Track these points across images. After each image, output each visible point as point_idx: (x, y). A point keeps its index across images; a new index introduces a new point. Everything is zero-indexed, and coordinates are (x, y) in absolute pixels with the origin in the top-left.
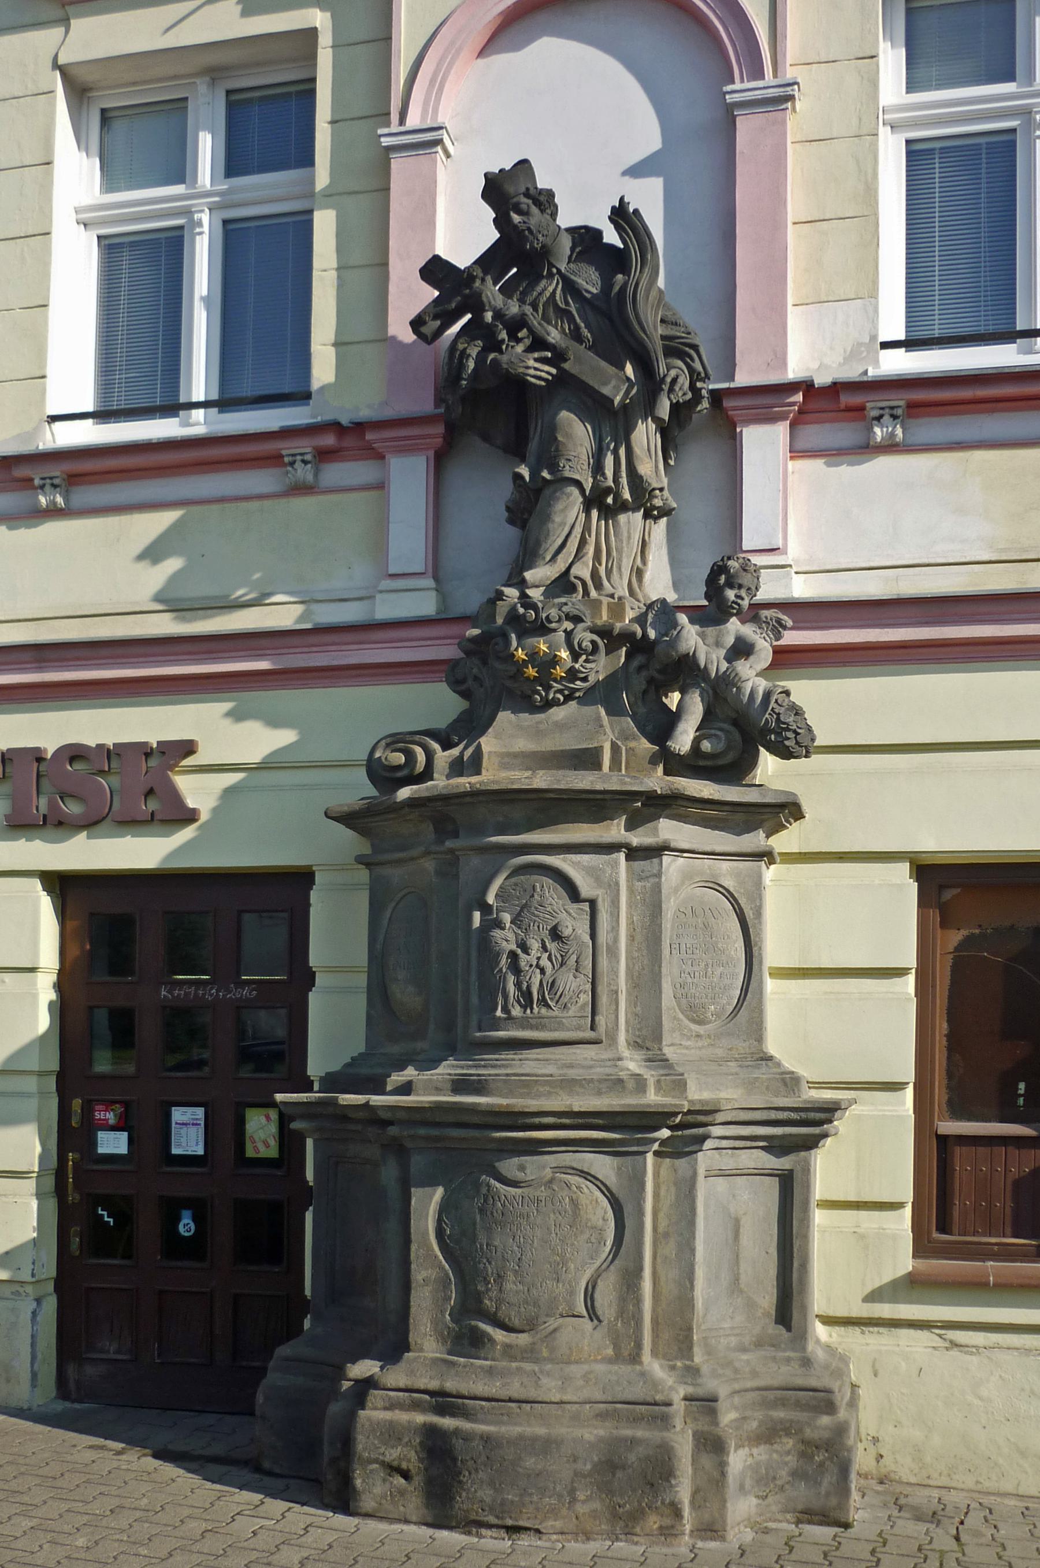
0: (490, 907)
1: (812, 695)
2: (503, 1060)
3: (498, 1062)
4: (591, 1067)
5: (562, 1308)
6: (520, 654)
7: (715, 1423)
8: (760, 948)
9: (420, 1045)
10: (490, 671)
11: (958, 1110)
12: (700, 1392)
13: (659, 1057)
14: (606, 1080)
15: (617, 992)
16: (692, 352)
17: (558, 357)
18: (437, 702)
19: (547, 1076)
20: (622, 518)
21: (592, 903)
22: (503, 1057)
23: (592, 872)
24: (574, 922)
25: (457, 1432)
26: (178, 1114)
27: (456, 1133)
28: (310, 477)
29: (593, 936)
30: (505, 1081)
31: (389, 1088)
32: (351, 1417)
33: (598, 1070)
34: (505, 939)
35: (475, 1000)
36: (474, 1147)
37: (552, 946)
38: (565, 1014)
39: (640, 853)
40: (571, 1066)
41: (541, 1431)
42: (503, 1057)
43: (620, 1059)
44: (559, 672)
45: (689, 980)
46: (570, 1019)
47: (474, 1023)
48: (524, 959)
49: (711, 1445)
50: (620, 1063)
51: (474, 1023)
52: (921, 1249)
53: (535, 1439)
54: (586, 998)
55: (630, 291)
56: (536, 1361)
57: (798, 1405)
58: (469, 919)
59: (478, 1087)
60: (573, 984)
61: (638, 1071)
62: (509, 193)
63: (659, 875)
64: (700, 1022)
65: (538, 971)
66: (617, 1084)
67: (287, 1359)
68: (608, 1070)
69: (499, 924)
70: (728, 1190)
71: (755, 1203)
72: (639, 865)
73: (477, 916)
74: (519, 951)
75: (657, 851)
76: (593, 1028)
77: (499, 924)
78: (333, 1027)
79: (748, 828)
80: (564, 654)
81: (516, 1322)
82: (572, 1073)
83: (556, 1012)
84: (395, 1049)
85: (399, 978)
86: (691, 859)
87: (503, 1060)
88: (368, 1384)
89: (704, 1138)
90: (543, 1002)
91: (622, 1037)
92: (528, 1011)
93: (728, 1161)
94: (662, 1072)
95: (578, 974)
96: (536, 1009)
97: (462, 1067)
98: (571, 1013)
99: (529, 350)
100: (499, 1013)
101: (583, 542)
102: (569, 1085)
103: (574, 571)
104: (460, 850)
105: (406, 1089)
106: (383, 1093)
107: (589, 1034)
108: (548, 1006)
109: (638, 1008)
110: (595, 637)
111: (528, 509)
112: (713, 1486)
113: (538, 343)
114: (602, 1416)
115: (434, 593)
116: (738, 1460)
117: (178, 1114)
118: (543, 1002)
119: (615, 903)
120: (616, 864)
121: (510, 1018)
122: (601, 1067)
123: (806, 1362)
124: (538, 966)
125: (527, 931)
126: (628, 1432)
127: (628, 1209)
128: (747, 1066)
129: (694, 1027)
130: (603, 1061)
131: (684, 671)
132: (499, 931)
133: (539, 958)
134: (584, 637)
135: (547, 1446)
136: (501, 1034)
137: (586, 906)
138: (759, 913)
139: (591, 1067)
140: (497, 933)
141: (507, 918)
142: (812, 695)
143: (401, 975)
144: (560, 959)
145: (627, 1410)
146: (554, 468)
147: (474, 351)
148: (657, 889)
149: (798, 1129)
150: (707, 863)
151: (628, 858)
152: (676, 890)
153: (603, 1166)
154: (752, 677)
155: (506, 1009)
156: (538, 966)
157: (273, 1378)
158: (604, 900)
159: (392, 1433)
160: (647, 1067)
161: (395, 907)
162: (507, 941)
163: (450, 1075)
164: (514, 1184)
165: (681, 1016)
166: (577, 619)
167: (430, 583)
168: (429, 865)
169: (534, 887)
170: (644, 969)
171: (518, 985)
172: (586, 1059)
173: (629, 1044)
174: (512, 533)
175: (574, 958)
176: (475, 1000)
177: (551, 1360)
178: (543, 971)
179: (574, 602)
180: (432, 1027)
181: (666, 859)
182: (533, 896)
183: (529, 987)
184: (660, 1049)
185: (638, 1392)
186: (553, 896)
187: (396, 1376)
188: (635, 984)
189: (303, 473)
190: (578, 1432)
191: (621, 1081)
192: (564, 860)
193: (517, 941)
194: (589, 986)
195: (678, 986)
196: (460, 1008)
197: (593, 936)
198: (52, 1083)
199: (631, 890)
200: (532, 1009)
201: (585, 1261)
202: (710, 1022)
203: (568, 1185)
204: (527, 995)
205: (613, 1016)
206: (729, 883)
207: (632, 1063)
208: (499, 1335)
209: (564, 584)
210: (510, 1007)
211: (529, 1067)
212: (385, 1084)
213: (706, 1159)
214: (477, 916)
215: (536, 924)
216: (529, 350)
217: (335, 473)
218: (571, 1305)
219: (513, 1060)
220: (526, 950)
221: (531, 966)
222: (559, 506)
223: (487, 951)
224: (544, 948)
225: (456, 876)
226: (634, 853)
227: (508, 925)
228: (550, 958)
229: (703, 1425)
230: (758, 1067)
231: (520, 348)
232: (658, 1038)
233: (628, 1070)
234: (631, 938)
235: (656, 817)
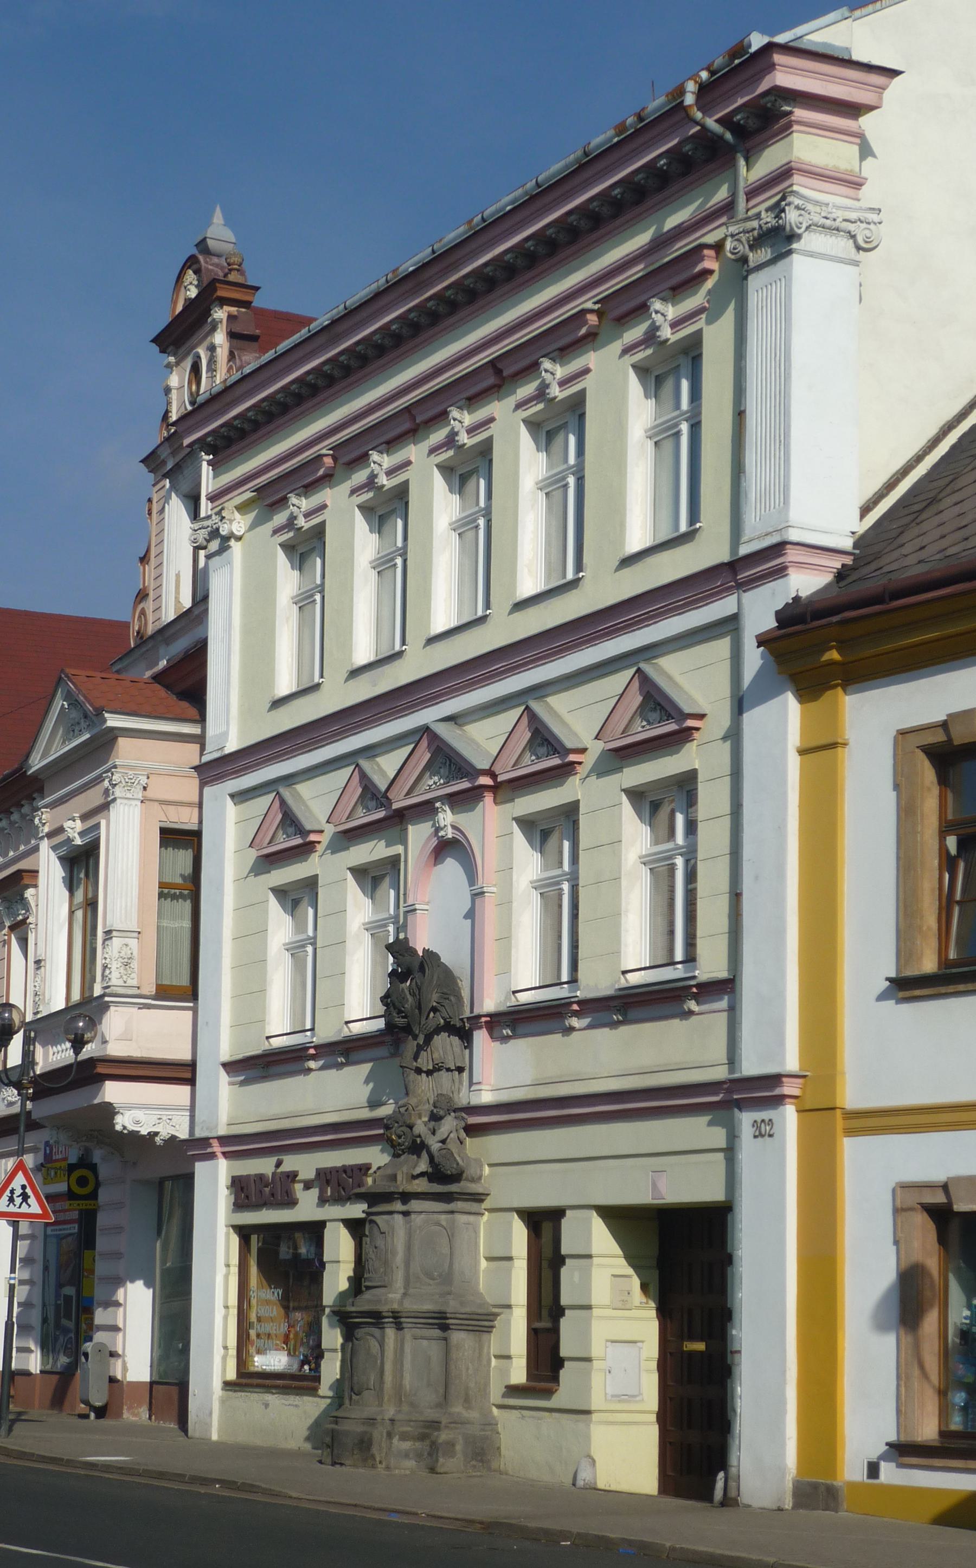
23: (387, 1222)
114: (363, 1424)
153: (376, 1331)
181: (413, 1216)
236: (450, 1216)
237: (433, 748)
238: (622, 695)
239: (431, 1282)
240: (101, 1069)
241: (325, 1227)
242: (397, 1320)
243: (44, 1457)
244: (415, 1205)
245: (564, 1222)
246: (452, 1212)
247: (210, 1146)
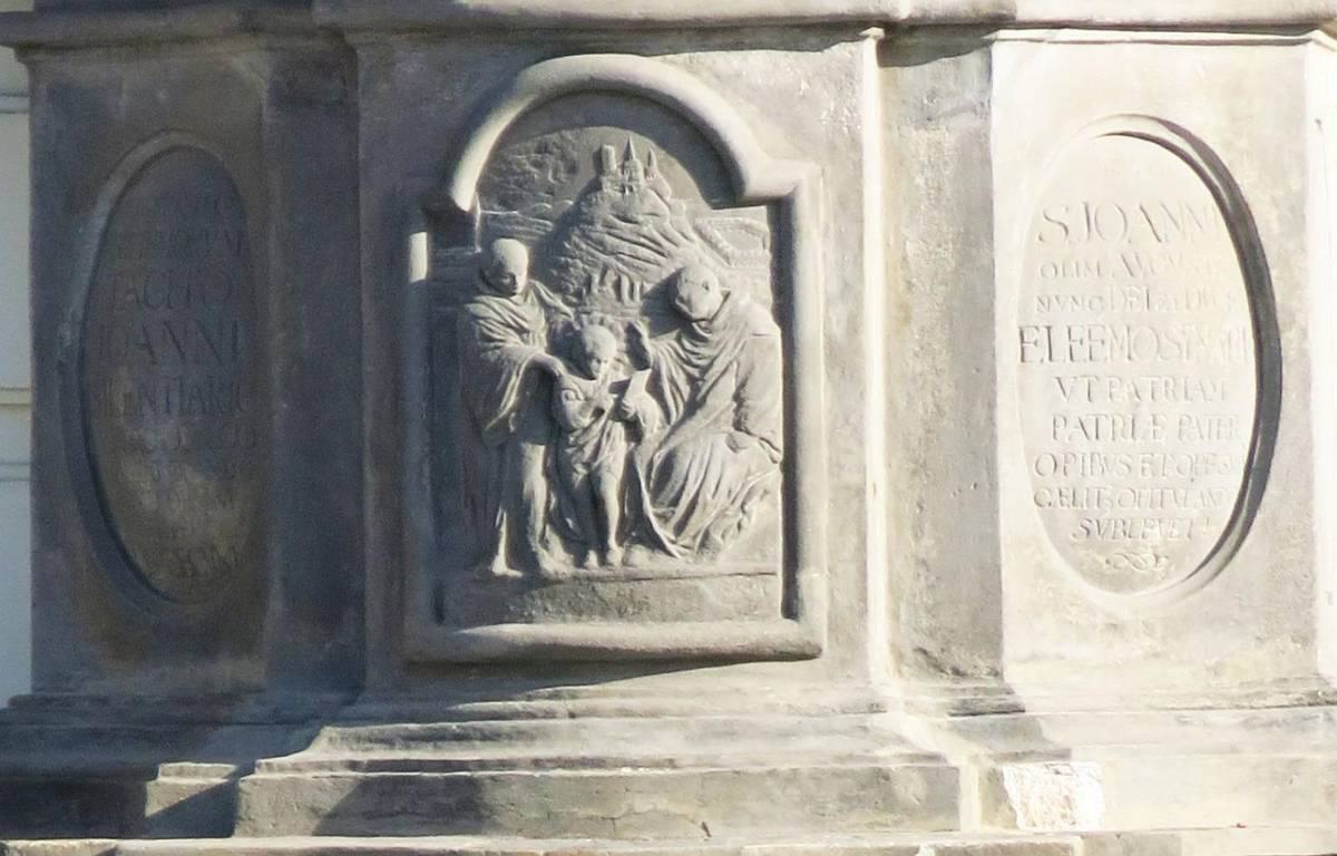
0: (464, 219)
2: (516, 715)
3: (505, 725)
4: (785, 735)
8: (1304, 333)
9: (227, 670)
13: (993, 701)
14: (836, 774)
15: (860, 492)
19: (658, 765)
21: (781, 210)
22: (518, 705)
23: (779, 107)
24: (723, 267)
29: (785, 311)
30: (531, 784)
31: (152, 809)
33: (812, 743)
34: (518, 325)
35: (421, 520)
37: (661, 348)
38: (704, 566)
39: (921, 39)
40: (729, 732)
42: (518, 705)
43: (875, 708)
45: (1083, 446)
46: (712, 582)
47: (420, 598)
48: (576, 393)
50: (876, 718)
51: (420, 598)
54: (767, 512)
60: (729, 469)
61: (930, 747)
63: (982, 109)
64: (1118, 581)
65: (619, 429)
68: (843, 745)
69: (496, 280)
72: (914, 77)
73: (420, 243)
74: (559, 367)
76: (791, 609)
77: (496, 280)
82: (730, 754)
84: (148, 683)
85: (152, 439)
87: (516, 715)
90: (639, 531)
91: (879, 632)
92: (593, 558)
94: (1004, 747)
95: (740, 436)
96: (616, 552)
97: (388, 742)
98: (723, 562)
100: (500, 566)
104: (356, 30)
107: (782, 631)
108: (655, 544)
109: (927, 542)
118: (639, 531)
119: (849, 204)
120: (847, 79)
121: (535, 580)
122: (819, 732)
124: (619, 413)
125: (580, 299)
128: (1270, 724)
130: (823, 712)
132: (494, 301)
133: (621, 388)
136: (514, 631)
137: (758, 218)
138: (1296, 218)
139: (785, 735)
140: (491, 309)
141: (517, 255)
143: (161, 432)
144: (686, 389)
145: (1001, 719)
148: (976, 156)
151: (889, 53)
155: (523, 554)
156: (619, 413)
158: (814, 197)
160: (956, 729)
161: (119, 201)
162: (521, 331)
163: (353, 765)
165: (1057, 562)
167: (25, 103)
168: (250, 64)
169: (599, 160)
170: (940, 411)
171: (557, 473)
172: (771, 708)
173: (899, 657)
175: (729, 385)
176: (421, 520)
178: (634, 430)
180: (276, 605)
181: (1007, 49)
182: (596, 186)
183: (593, 480)
184: (997, 674)
186: (661, 190)
188: (918, 464)
191: (881, 777)
192: (691, 69)
193: (552, 334)
194: (775, 477)
195: (1047, 465)
196: (373, 550)
197: (785, 311)
199: (897, 161)
200: (603, 551)
202: (1148, 581)
205: (852, 568)
207: (915, 719)
210: (536, 546)
211: (601, 737)
212: (141, 798)
214: (420, 243)
215: (611, 277)
219: (550, 715)
220: (582, 362)
221: (599, 412)
224: (638, 357)
225: (346, 111)
227: (522, 281)
228: (655, 388)
230: (1302, 725)
232: (989, 638)
233: (901, 740)
234: (901, 315)
236: (1266, 58)
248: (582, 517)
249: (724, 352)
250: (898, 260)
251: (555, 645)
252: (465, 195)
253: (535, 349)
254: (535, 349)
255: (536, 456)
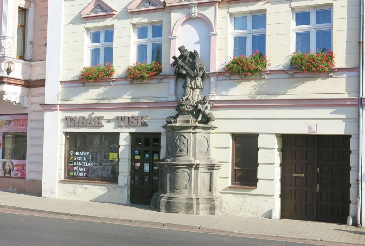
1: (216, 114)
5: (183, 188)
6: (181, 108)
7: (199, 201)
10: (180, 109)
11: (236, 166)
12: (198, 198)
16: (203, 69)
17: (187, 71)
18: (173, 112)
20: (195, 90)
21: (188, 139)
23: (188, 136)
24: (185, 142)
25: (171, 201)
26: (145, 164)
27: (172, 166)
28: (161, 81)
29: (188, 143)
32: (160, 200)
34: (178, 143)
36: (174, 168)
40: (185, 159)
41: (179, 201)
44: (186, 111)
46: (184, 153)
49: (198, 204)
52: (232, 183)
53: (178, 202)
55: (195, 62)
56: (180, 194)
57: (210, 201)
58: (175, 141)
59: (175, 161)
60: (185, 149)
62: (181, 49)
66: (189, 161)
67: (155, 195)
70: (203, 175)
71: (207, 176)
75: (195, 133)
76: (187, 154)
78: (163, 152)
79: (208, 129)
80: (186, 109)
81: (178, 189)
82: (184, 160)
83: (183, 152)
86: (200, 134)
88: (162, 196)
89: (199, 168)
93: (203, 171)
99: (184, 70)
101: (190, 93)
102: (184, 161)
103: (189, 98)
105: (167, 161)
106: (165, 162)
110: (190, 107)
111: (185, 87)
112: (198, 209)
113: (184, 69)
114: (186, 200)
115: (175, 98)
116: (201, 206)
117: (145, 164)
118: (182, 151)
120: (190, 134)
123: (212, 196)
126: (188, 202)
127: (190, 176)
129: (201, 154)
131: (200, 111)
134: (189, 106)
135: (179, 203)
136: (177, 155)
138: (209, 140)
140: (177, 143)
141: (178, 141)
142: (216, 114)
146: (186, 85)
147: (177, 70)
149: (211, 168)
150: (203, 134)
152: (198, 137)
153: (188, 171)
154: (207, 112)
157: (154, 197)
159: (164, 201)
164: (178, 173)
166: (188, 104)
167: (175, 96)
171: (179, 149)
174: (184, 90)
177: (181, 193)
179: (187, 102)
181: (197, 134)
185: (190, 197)
186: (183, 138)
187: (165, 195)
189: (161, 81)
190: (183, 202)
197: (188, 143)
198: (130, 160)
201: (185, 182)
203: (183, 173)
204: (180, 150)
206: (206, 136)
208: (176, 191)
209: (187, 99)
213: (200, 171)
216: (184, 70)
217: (164, 80)
218: (184, 187)
220: (180, 145)
222: (187, 89)
223: (176, 145)
226: (193, 133)
229: (197, 201)
231: (182, 70)
232: (196, 155)
234: (193, 143)
235: (196, 129)
236: (208, 134)
237: (96, 4)
238: (90, 4)
239: (202, 155)
240: (4, 80)
241: (259, 136)
242: (197, 167)
243: (352, 233)
244: (197, 130)
245: (120, 136)
246: (209, 133)
247: (57, 107)
248: (180, 150)
249: (185, 145)
250: (193, 141)
251: (86, 92)
252: (177, 138)
253: (179, 144)
254: (179, 144)
255: (178, 148)
